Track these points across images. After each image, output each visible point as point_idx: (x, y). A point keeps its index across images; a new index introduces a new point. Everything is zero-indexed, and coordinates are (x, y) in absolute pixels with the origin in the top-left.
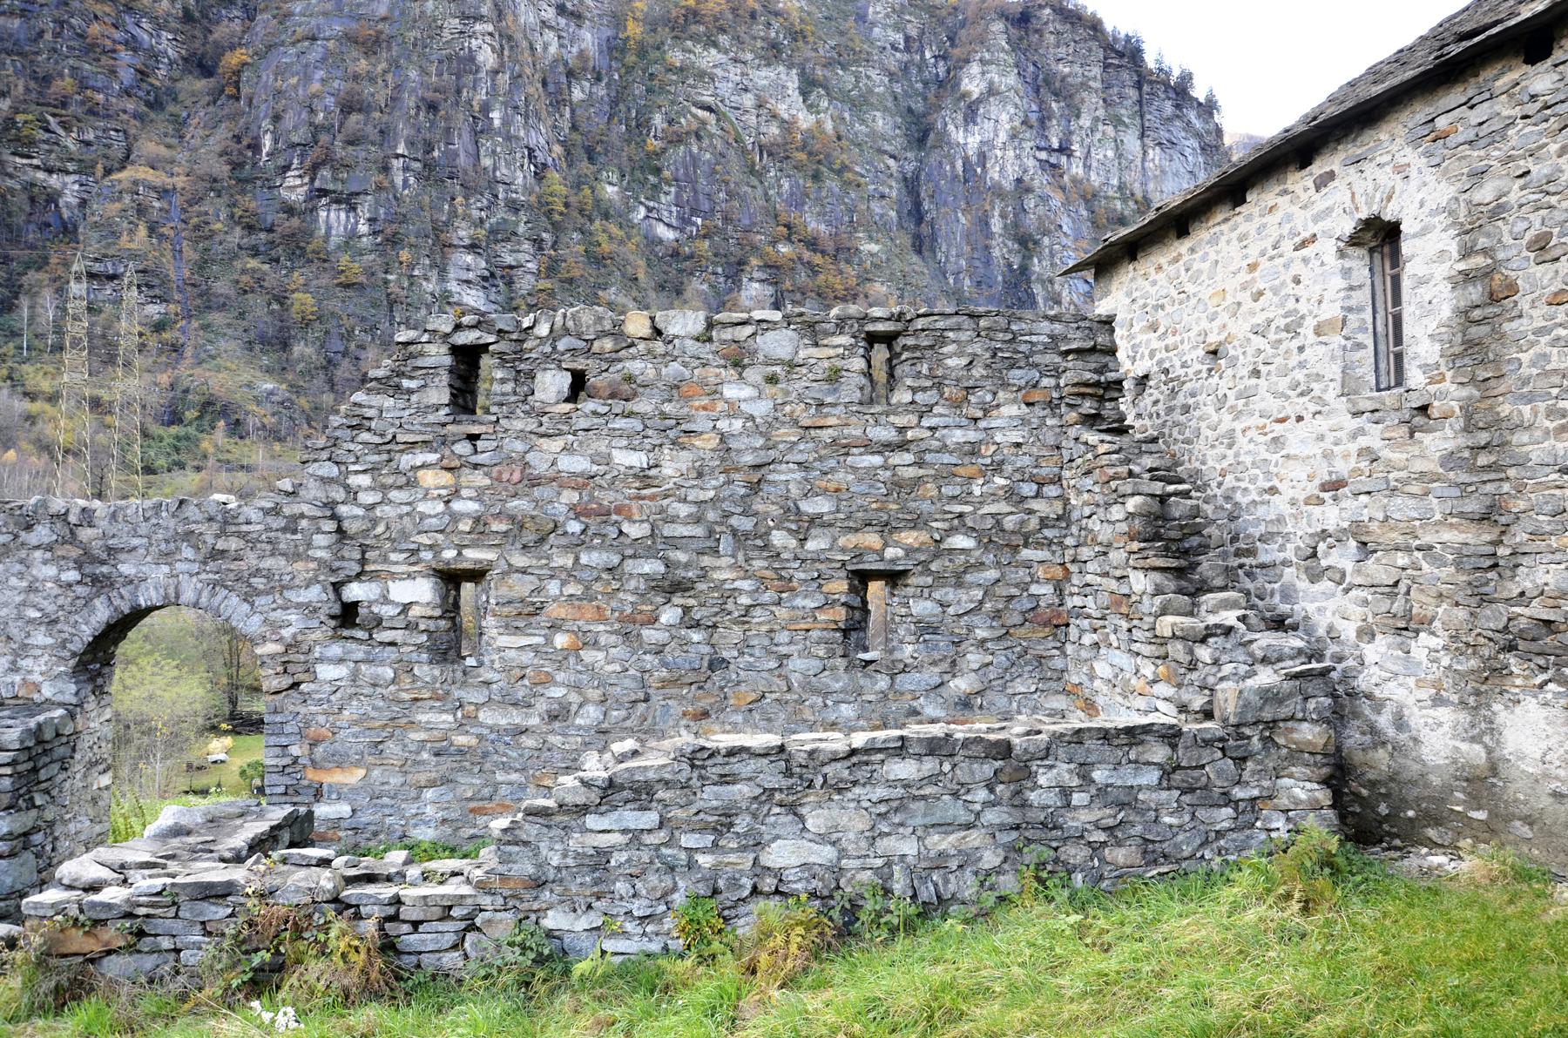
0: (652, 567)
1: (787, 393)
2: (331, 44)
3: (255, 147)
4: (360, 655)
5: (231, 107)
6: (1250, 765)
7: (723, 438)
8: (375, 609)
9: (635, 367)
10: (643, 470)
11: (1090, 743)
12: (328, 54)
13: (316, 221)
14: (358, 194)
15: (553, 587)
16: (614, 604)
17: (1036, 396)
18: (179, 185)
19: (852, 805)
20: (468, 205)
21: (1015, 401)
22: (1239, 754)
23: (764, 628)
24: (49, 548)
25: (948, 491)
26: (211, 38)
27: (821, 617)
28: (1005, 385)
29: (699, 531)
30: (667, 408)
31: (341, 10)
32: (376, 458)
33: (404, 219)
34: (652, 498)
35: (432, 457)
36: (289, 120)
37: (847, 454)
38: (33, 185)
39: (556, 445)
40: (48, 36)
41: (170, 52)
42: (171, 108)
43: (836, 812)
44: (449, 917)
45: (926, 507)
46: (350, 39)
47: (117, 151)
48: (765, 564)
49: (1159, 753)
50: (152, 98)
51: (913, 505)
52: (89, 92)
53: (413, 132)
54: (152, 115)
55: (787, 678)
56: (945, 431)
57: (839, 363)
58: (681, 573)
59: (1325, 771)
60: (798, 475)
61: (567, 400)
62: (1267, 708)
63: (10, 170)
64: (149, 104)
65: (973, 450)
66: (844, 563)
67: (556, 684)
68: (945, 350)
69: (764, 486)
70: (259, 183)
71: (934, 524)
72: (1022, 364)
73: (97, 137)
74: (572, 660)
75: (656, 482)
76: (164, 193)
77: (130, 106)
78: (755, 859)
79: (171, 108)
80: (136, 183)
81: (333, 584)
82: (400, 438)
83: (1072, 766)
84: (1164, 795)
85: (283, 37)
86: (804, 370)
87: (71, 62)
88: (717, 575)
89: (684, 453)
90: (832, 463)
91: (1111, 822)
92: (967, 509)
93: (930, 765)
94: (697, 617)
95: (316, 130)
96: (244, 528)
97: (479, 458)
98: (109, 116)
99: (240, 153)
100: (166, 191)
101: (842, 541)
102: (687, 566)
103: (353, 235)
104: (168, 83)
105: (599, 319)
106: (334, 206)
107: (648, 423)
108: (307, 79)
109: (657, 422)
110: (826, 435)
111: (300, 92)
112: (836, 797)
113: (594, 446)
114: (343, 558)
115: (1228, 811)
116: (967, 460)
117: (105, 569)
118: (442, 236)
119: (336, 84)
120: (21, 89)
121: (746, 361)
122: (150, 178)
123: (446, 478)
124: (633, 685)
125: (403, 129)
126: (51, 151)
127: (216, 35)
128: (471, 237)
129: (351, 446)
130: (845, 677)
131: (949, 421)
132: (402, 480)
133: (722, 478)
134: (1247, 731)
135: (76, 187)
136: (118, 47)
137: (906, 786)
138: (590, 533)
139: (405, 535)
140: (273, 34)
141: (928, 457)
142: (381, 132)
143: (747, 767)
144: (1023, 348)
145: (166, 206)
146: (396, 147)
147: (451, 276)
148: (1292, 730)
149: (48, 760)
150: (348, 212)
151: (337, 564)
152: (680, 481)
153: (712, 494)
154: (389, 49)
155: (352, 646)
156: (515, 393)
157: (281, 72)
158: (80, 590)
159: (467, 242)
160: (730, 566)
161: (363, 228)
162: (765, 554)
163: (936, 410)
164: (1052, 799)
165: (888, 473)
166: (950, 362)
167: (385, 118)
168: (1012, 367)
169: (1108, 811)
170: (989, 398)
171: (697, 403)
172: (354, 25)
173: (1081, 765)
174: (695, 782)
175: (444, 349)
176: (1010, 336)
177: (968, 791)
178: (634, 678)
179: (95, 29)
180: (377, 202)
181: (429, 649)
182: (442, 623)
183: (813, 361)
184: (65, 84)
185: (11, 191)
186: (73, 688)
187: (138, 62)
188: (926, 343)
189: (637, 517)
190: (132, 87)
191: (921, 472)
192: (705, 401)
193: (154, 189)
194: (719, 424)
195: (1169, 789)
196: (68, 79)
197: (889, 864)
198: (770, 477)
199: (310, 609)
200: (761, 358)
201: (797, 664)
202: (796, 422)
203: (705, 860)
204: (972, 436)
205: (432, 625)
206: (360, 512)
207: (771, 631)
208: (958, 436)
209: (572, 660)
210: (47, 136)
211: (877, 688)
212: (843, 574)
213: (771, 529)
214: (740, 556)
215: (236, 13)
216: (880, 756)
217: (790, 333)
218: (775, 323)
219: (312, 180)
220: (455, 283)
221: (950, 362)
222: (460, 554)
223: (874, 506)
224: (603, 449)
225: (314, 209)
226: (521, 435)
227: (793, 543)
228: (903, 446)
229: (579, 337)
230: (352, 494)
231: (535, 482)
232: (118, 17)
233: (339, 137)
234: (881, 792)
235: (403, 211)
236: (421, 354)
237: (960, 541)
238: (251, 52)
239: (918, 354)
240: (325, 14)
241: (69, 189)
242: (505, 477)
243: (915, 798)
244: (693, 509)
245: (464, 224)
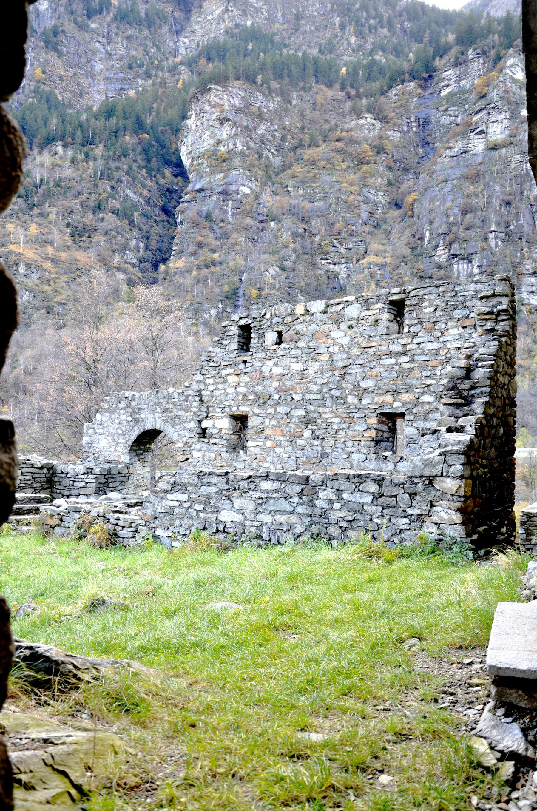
0: (302, 413)
1: (356, 333)
2: (455, 182)
3: (421, 239)
4: (205, 449)
5: (409, 221)
6: (417, 497)
7: (331, 355)
8: (211, 431)
9: (299, 327)
10: (301, 371)
11: (341, 481)
12: (454, 186)
13: (453, 270)
14: (472, 254)
15: (267, 421)
16: (287, 429)
17: (467, 323)
18: (388, 262)
19: (249, 499)
20: (530, 252)
21: (456, 326)
22: (410, 491)
23: (343, 440)
24: (124, 409)
25: (425, 374)
26: (400, 191)
27: (366, 434)
28: (451, 318)
29: (319, 397)
30: (311, 344)
31: (459, 164)
32: (214, 372)
33: (497, 263)
34: (305, 383)
35: (231, 371)
36: (437, 223)
37: (381, 359)
38: (328, 271)
39: (270, 363)
40: (333, 206)
41: (382, 201)
42: (384, 227)
43: (243, 501)
44: (131, 527)
45: (414, 382)
46: (465, 177)
47: (362, 251)
48: (343, 410)
49: (373, 488)
50: (375, 224)
51: (408, 381)
52: (349, 226)
53: (498, 219)
54: (376, 231)
55: (351, 463)
56: (423, 345)
57: (377, 317)
58: (311, 415)
59: (458, 505)
60: (360, 370)
61: (276, 344)
62: (426, 469)
63: (320, 266)
64: (375, 227)
65: (437, 352)
66: (375, 409)
67: (266, 462)
68: (423, 305)
69: (347, 376)
70: (424, 255)
71: (417, 390)
72: (460, 307)
73: (353, 246)
74: (272, 452)
75: (306, 376)
76: (381, 266)
77: (366, 229)
78: (217, 517)
79: (384, 227)
80: (369, 264)
81: (199, 421)
82: (222, 364)
83: (333, 490)
84: (374, 508)
85: (432, 183)
86: (363, 322)
87: (342, 214)
88: (325, 416)
89: (317, 363)
90: (374, 363)
91: (350, 519)
92: (434, 382)
93: (276, 485)
94: (317, 434)
95: (450, 225)
96: (173, 400)
97: (247, 370)
98: (357, 235)
99: (415, 243)
100: (383, 265)
101: (376, 400)
102: (314, 412)
103: (471, 275)
104: (382, 215)
105: (286, 309)
106: (461, 262)
107: (304, 351)
108: (444, 201)
109: (307, 351)
110: (372, 351)
111: (442, 208)
112: (243, 495)
113: (285, 362)
114: (201, 411)
115: (406, 520)
116: (433, 358)
117: (137, 416)
118: (517, 270)
119: (458, 201)
120: (323, 230)
121: (340, 320)
122: (375, 260)
123: (236, 379)
124: (293, 463)
125: (494, 218)
126: (335, 255)
127: (402, 189)
128: (533, 268)
129: (207, 368)
130: (374, 463)
131: (426, 339)
132: (222, 380)
133: (330, 373)
134: (416, 480)
135: (345, 269)
136: (361, 204)
137: (268, 493)
138: (282, 399)
139: (221, 401)
140: (427, 183)
141: (416, 358)
142: (483, 221)
143: (215, 480)
144: (461, 299)
145: (383, 273)
146: (490, 227)
147: (523, 290)
148: (443, 482)
149: (113, 480)
150: (468, 264)
151: (199, 413)
152: (314, 375)
153: (326, 380)
154: (484, 178)
155: (204, 445)
156: (258, 343)
157: (432, 200)
158: (132, 423)
159: (531, 271)
160: (330, 412)
161: (476, 271)
162: (344, 406)
163: (420, 334)
164: (326, 506)
165: (398, 367)
166: (426, 311)
167: (484, 213)
168: (455, 309)
169: (348, 513)
170: (443, 326)
171: (321, 341)
172: (466, 170)
173: (338, 490)
174: (199, 485)
175: (236, 328)
176: (454, 294)
177: (291, 497)
178: (293, 460)
179: (352, 197)
180: (482, 257)
181: (227, 447)
182: (233, 436)
183: (366, 317)
184: (340, 225)
185: (320, 275)
186: (129, 458)
187: (369, 209)
188: (415, 303)
189: (298, 392)
190: (367, 220)
191: (412, 365)
192: (324, 340)
193: (377, 265)
194: (330, 349)
195: (377, 505)
196: (341, 223)
197: (261, 525)
198: (349, 372)
199: (191, 430)
200: (346, 318)
201: (355, 456)
202: (360, 345)
203: (202, 515)
204: (436, 346)
205: (228, 437)
206: (209, 393)
207: (345, 441)
208: (429, 346)
209: (272, 452)
210: (333, 248)
211: (388, 469)
212: (375, 415)
213: (347, 395)
214: (334, 408)
215: (411, 177)
216: (259, 479)
217: (358, 305)
218: (352, 302)
219: (450, 250)
220: (525, 294)
221: (426, 311)
222: (238, 409)
223: (391, 383)
224: (288, 363)
225: (451, 265)
226: (261, 360)
227: (356, 401)
228: (404, 354)
229: (279, 317)
230: (206, 385)
231: (264, 379)
232: (360, 190)
233: (461, 227)
234: (258, 495)
235: (496, 259)
236: (230, 330)
237: (426, 398)
238: (417, 193)
239: (412, 308)
240: (452, 168)
241: (342, 270)
242: (254, 377)
243: (271, 498)
244: (319, 387)
245: (529, 262)
